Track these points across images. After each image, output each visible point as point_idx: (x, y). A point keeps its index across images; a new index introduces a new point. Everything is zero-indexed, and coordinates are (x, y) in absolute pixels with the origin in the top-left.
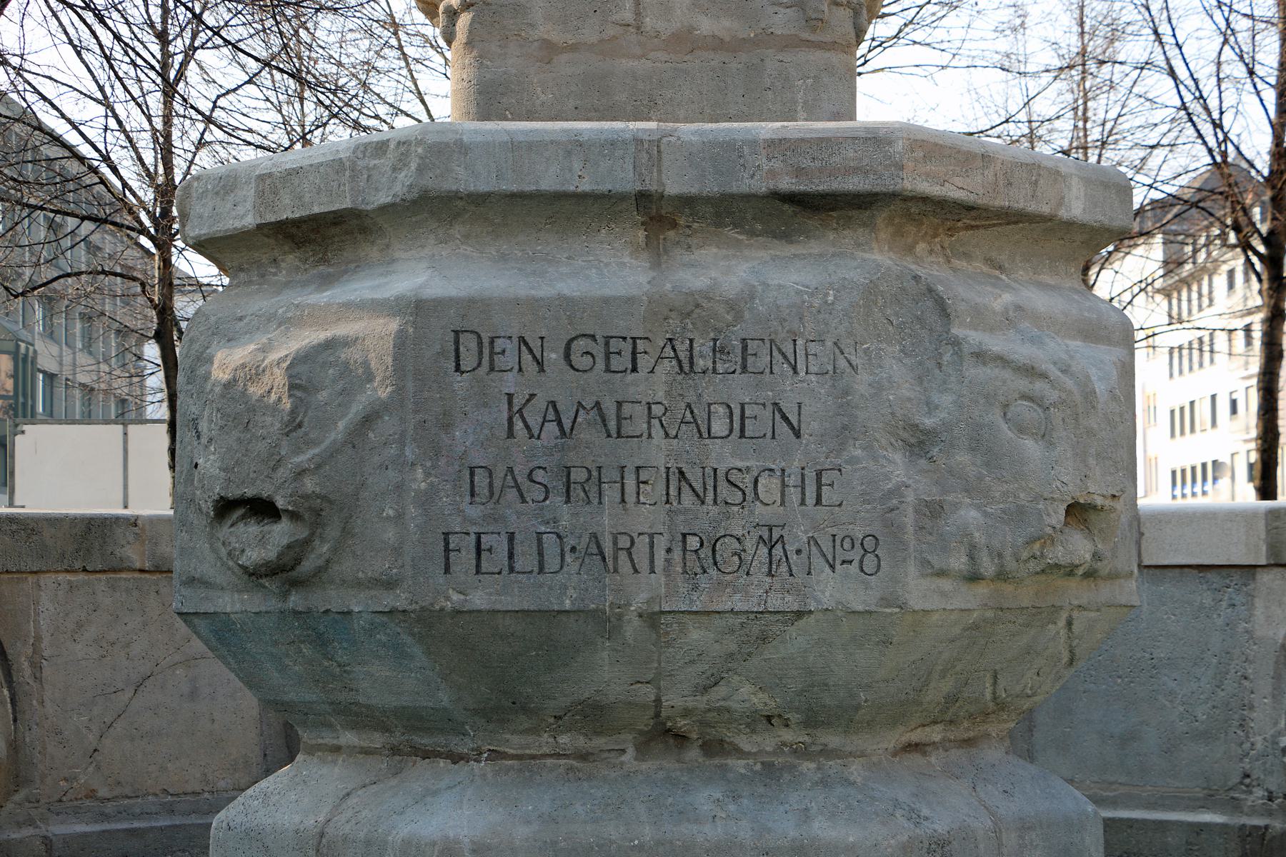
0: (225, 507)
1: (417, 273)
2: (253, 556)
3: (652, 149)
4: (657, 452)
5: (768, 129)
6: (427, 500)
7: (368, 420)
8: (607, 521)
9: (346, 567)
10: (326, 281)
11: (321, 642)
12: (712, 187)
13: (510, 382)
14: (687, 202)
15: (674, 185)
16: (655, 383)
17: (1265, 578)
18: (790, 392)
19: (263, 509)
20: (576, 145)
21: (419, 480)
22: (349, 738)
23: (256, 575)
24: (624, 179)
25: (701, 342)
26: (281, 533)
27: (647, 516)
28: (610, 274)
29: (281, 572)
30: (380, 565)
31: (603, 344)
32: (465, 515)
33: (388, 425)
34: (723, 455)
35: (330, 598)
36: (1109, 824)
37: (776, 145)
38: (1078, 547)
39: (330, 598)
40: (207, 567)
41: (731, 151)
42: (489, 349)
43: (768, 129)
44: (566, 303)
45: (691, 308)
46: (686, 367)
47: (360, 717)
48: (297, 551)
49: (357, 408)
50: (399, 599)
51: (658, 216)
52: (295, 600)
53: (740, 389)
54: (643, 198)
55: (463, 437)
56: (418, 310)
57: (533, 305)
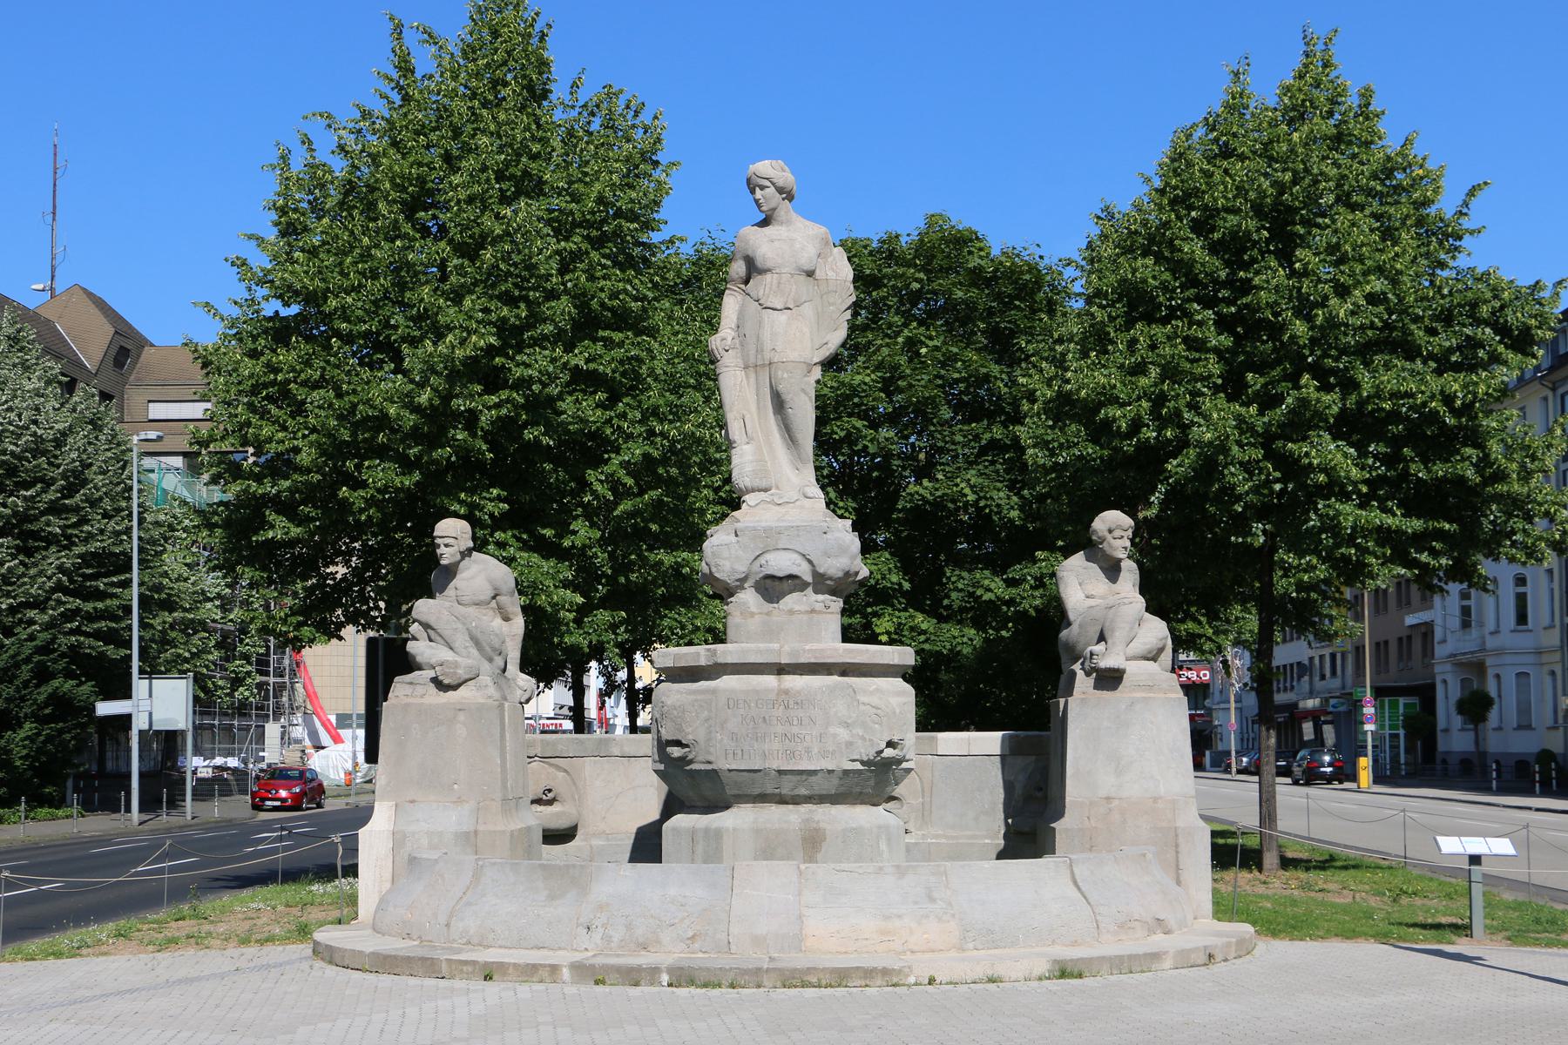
20: (760, 652)
34: (795, 730)
51: (781, 670)
53: (801, 713)
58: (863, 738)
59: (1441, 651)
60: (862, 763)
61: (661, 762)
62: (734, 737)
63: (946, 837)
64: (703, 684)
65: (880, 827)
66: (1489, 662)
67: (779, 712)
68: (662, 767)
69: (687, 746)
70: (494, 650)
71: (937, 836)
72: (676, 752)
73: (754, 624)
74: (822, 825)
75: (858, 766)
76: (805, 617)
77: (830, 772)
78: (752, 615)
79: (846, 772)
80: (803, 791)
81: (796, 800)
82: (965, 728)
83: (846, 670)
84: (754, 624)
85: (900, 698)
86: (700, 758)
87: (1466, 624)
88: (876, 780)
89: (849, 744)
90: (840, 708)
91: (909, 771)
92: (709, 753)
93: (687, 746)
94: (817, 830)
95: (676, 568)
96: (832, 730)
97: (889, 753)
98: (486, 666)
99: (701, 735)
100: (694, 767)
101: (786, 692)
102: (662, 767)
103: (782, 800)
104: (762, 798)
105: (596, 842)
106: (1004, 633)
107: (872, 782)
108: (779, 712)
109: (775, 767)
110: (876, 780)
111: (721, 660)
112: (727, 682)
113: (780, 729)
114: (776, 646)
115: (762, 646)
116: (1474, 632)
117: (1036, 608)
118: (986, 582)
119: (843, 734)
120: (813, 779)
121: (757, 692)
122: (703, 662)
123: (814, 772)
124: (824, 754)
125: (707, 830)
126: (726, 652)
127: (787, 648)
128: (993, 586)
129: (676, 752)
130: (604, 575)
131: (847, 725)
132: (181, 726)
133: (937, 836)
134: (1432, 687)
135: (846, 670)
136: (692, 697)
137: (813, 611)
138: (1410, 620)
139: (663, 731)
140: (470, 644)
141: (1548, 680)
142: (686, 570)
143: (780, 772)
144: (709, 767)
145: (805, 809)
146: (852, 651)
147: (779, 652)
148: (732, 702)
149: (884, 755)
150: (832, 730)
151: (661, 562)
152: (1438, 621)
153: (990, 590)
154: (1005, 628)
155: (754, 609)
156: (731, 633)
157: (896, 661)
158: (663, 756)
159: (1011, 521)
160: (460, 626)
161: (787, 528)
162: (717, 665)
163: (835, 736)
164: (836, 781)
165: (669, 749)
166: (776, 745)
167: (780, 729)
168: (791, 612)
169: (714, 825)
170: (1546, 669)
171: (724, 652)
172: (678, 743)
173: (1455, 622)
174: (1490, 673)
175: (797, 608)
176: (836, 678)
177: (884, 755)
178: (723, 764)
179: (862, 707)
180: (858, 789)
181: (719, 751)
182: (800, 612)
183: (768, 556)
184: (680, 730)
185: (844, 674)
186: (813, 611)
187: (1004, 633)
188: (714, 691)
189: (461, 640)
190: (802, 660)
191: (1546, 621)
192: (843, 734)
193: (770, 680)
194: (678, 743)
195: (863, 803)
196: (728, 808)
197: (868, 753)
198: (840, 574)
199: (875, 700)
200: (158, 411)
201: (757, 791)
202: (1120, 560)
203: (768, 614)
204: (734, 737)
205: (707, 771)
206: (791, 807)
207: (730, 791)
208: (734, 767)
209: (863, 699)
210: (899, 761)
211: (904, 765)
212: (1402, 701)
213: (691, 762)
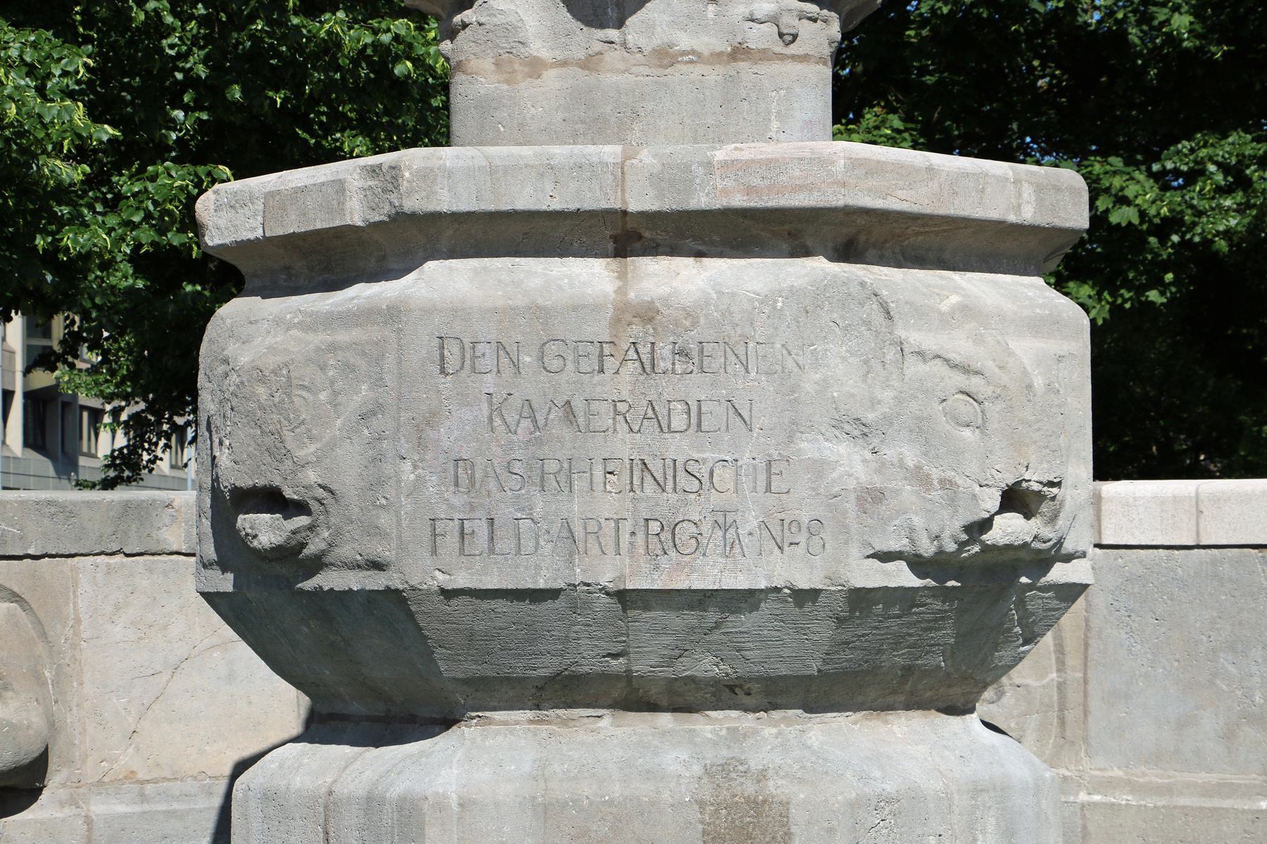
20: (550, 169)
34: (679, 447)
51: (626, 236)
53: (696, 388)
58: (920, 478)
60: (918, 564)
61: (223, 565)
62: (461, 472)
63: (1134, 787)
64: (361, 293)
65: (976, 790)
67: (623, 382)
68: (225, 583)
69: (299, 508)
71: (1109, 785)
72: (265, 530)
73: (543, 95)
74: (776, 787)
75: (902, 576)
76: (713, 75)
77: (805, 597)
78: (535, 67)
79: (860, 599)
80: (705, 666)
81: (683, 698)
82: (330, 743)
83: (857, 236)
84: (543, 95)
85: (1040, 339)
86: (346, 551)
88: (959, 621)
89: (872, 498)
90: (838, 370)
91: (1071, 592)
92: (375, 531)
93: (299, 508)
94: (757, 805)
95: (382, 58)
96: (808, 447)
97: (1010, 529)
99: (347, 469)
100: (328, 580)
101: (647, 314)
102: (225, 583)
103: (635, 697)
104: (564, 691)
105: (100, 808)
106: (1153, 295)
107: (947, 634)
108: (623, 382)
109: (606, 577)
110: (959, 621)
111: (414, 203)
112: (442, 282)
114: (611, 152)
115: (560, 152)
117: (1227, 234)
118: (1117, 182)
119: (850, 462)
120: (745, 621)
121: (539, 313)
122: (356, 213)
123: (746, 599)
124: (781, 534)
125: (372, 803)
126: (433, 176)
127: (646, 158)
128: (1130, 191)
129: (265, 530)
130: (191, 81)
131: (862, 431)
133: (1109, 785)
135: (857, 236)
136: (320, 338)
137: (739, 52)
139: (224, 458)
142: (404, 68)
143: (625, 598)
144: (376, 581)
145: (713, 726)
146: (876, 169)
147: (621, 172)
148: (454, 351)
149: (991, 537)
150: (808, 447)
151: (334, 42)
153: (1122, 200)
154: (1158, 283)
155: (539, 48)
156: (460, 122)
157: (1028, 214)
158: (230, 549)
159: (1173, 40)
162: (403, 221)
163: (819, 468)
164: (823, 631)
165: (246, 521)
167: (623, 446)
168: (666, 57)
169: (397, 789)
171: (426, 175)
172: (271, 500)
175: (685, 41)
176: (819, 266)
177: (991, 537)
178: (423, 571)
179: (914, 368)
180: (900, 658)
181: (409, 533)
182: (696, 57)
184: (278, 452)
185: (847, 252)
186: (739, 52)
187: (1153, 295)
188: (392, 314)
190: (702, 200)
192: (850, 462)
193: (590, 276)
194: (271, 500)
195: (914, 703)
196: (446, 722)
197: (937, 528)
199: (959, 344)
201: (546, 667)
203: (589, 63)
204: (461, 472)
205: (370, 597)
206: (665, 720)
207: (450, 667)
208: (461, 580)
209: (916, 337)
210: (1041, 558)
211: (1059, 573)
213: (317, 564)
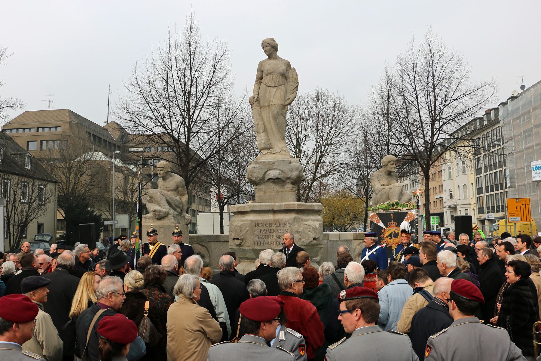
0: (234, 239)
1: (251, 217)
2: (237, 243)
3: (273, 206)
4: (274, 234)
5: (284, 203)
6: (253, 239)
7: (247, 231)
8: (269, 240)
9: (246, 245)
10: (243, 217)
11: (243, 252)
12: (279, 209)
13: (260, 228)
14: (277, 210)
15: (275, 209)
16: (274, 228)
17: (353, 241)
18: (286, 228)
19: (238, 239)
20: (266, 205)
21: (252, 237)
22: (246, 261)
23: (237, 245)
24: (271, 208)
25: (277, 223)
26: (239, 241)
27: (273, 240)
28: (270, 217)
29: (239, 245)
30: (249, 245)
31: (269, 224)
32: (256, 240)
33: (249, 232)
34: (280, 234)
35: (244, 248)
36: (143, 255)
37: (285, 205)
38: (315, 242)
39: (244, 248)
40: (232, 244)
41: (281, 206)
42: (258, 225)
43: (284, 203)
44: (266, 220)
45: (277, 220)
46: (277, 226)
47: (247, 259)
48: (241, 243)
49: (246, 230)
50: (250, 248)
51: (274, 212)
52: (241, 248)
53: (282, 228)
54: (273, 210)
55: (256, 233)
56: (252, 221)
57: (263, 220)
59: (445, 205)
66: (458, 207)
70: (177, 206)
87: (451, 197)
98: (172, 211)
113: (274, 234)
116: (453, 199)
132: (126, 227)
134: (443, 214)
138: (437, 197)
140: (166, 204)
141: (473, 211)
152: (444, 197)
160: (163, 198)
161: (276, 161)
166: (273, 240)
170: (472, 208)
173: (449, 197)
174: (458, 210)
177: (313, 243)
183: (269, 172)
189: (164, 202)
191: (472, 196)
198: (295, 177)
200: (132, 149)
202: (122, 276)
212: (435, 217)
